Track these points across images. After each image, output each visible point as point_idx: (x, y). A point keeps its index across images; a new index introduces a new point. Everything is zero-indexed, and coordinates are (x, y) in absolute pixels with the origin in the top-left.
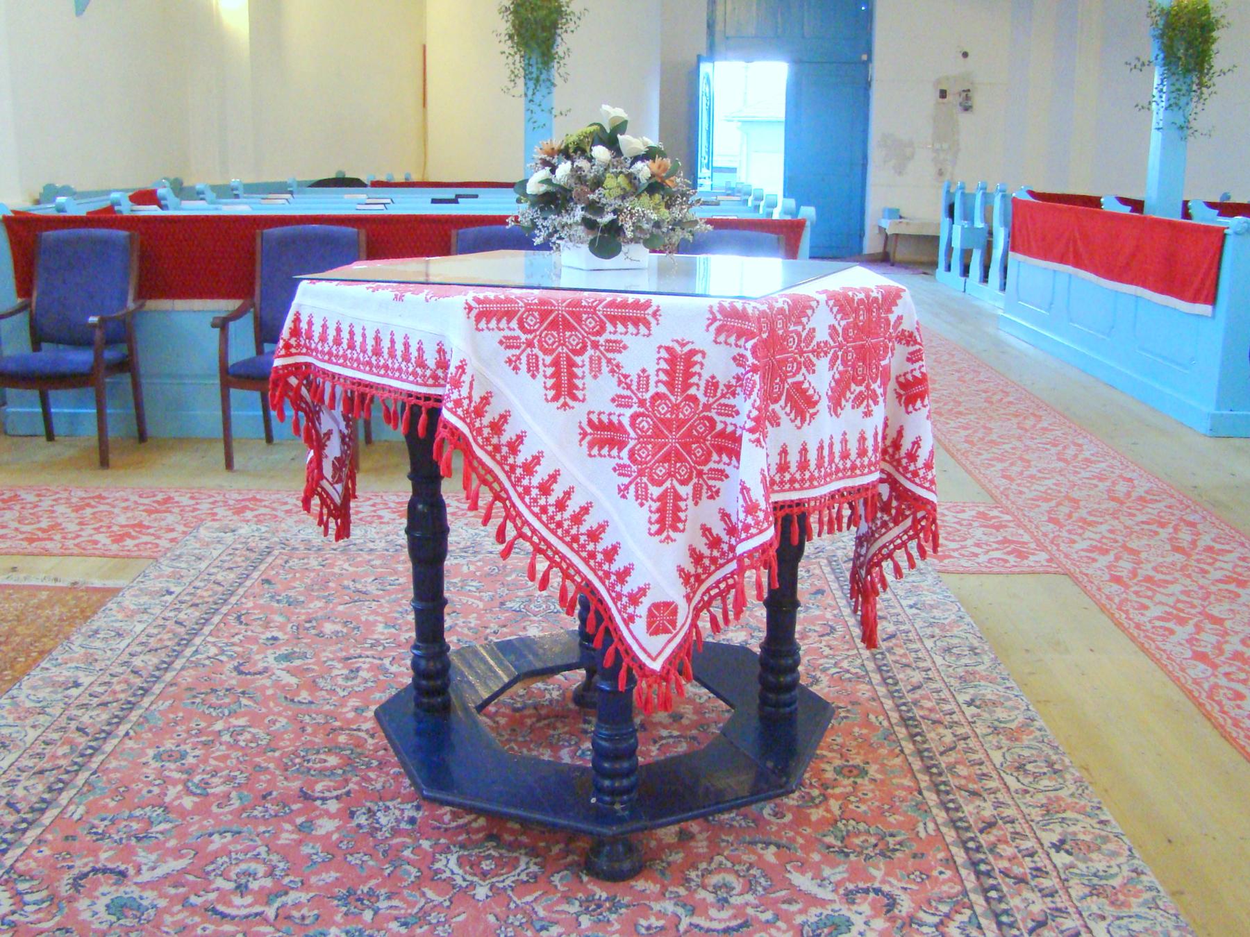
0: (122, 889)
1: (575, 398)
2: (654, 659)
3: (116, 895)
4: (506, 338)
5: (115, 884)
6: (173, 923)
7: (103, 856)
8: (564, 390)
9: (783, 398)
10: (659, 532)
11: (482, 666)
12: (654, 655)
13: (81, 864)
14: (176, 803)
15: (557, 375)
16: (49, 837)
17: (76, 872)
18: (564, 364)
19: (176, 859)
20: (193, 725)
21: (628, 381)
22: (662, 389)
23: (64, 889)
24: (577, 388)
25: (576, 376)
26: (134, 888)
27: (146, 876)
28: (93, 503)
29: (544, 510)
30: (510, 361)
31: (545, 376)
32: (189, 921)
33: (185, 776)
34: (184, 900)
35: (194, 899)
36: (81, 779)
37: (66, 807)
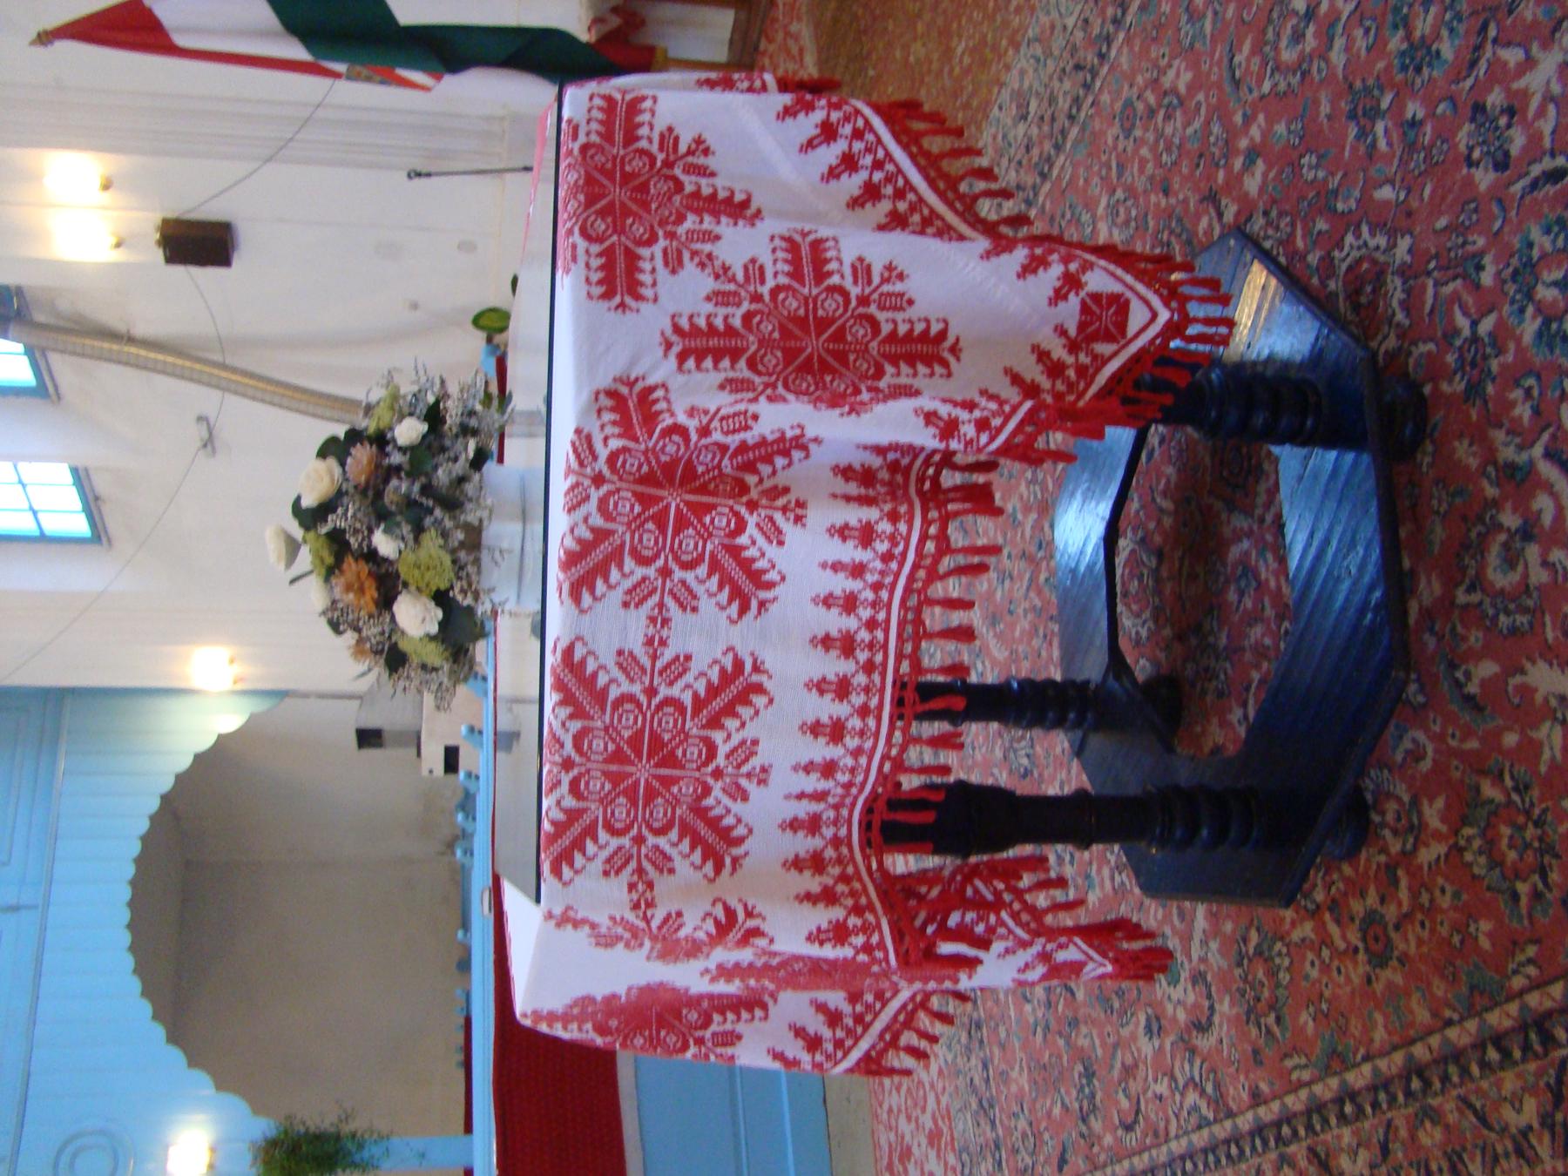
25: (709, 684)
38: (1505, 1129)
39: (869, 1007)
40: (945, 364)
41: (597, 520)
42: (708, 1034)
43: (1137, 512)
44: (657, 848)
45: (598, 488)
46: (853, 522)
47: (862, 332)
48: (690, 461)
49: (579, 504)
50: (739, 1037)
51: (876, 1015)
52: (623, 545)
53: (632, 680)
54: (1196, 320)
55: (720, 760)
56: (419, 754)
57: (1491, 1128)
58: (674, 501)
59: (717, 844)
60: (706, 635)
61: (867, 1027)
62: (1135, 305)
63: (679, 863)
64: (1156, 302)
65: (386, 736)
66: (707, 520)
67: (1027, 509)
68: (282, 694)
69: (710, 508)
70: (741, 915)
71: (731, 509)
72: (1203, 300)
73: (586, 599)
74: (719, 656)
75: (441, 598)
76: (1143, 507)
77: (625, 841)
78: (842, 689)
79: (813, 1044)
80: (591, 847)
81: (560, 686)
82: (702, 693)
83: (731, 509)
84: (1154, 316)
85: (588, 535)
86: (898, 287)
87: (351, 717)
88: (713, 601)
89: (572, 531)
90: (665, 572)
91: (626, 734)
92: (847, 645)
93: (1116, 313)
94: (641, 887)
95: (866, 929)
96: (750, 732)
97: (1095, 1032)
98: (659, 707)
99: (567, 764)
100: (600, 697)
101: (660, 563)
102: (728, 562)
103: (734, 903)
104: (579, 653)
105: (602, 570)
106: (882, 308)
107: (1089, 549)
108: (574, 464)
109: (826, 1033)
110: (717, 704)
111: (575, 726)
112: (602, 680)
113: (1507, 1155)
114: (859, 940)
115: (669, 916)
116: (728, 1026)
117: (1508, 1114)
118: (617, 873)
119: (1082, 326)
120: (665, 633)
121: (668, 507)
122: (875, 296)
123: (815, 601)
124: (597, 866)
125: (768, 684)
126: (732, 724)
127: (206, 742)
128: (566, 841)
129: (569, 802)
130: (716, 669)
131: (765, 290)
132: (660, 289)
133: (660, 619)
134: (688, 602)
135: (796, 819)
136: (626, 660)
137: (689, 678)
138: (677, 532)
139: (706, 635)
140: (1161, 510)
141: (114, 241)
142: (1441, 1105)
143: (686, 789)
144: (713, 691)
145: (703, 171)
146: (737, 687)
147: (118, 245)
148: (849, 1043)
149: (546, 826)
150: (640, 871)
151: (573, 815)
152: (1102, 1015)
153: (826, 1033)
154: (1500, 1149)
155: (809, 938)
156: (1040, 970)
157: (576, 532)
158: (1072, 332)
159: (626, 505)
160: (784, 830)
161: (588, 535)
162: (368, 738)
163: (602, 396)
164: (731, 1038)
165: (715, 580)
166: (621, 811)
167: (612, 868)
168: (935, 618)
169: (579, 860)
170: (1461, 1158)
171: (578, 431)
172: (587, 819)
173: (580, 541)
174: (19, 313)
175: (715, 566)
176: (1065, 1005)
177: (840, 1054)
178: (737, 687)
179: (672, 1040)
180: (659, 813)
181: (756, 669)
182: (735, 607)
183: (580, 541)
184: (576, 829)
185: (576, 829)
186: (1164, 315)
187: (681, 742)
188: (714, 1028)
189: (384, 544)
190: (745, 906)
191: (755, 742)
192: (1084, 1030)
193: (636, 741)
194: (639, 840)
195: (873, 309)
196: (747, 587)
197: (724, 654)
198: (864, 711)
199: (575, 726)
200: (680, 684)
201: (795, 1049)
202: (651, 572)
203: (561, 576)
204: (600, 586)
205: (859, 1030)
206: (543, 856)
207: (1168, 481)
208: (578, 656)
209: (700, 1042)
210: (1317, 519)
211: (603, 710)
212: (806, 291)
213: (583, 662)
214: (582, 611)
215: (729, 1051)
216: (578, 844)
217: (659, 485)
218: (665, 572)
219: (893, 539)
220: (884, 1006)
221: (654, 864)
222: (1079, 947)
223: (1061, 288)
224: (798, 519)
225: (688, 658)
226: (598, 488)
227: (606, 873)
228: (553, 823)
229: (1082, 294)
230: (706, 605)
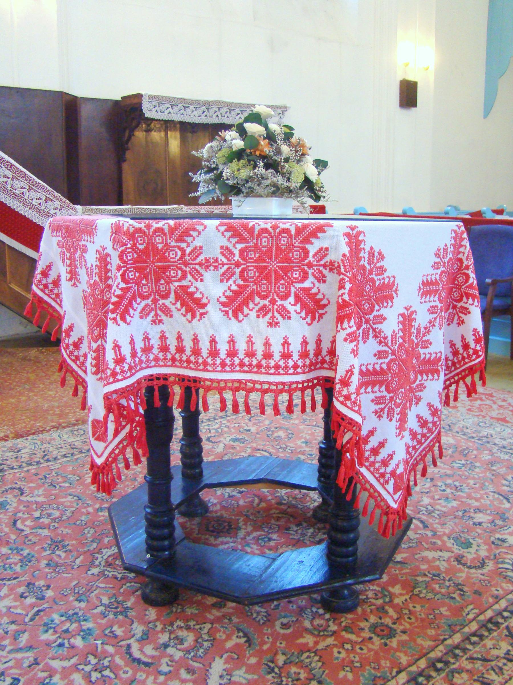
0: (461, 552)
2: (99, 457)
3: (465, 550)
4: (227, 248)
5: (464, 556)
6: (446, 529)
7: (463, 575)
8: (236, 304)
9: (256, 232)
12: (99, 454)
13: (477, 574)
14: (404, 592)
16: (491, 600)
17: (480, 571)
19: (426, 557)
20: (343, 655)
22: (240, 246)
23: (490, 566)
26: (454, 550)
27: (446, 555)
28: (484, 398)
29: (188, 361)
32: (439, 526)
33: (387, 607)
34: (435, 535)
35: (430, 534)
36: (457, 638)
37: (474, 619)
38: (498, 657)
40: (412, 313)
57: (493, 661)
60: (212, 287)
90: (238, 265)
113: (505, 664)
117: (495, 652)
125: (195, 321)
133: (207, 264)
134: (226, 276)
135: (198, 341)
139: (212, 287)
142: (460, 666)
145: (445, 250)
146: (193, 305)
154: (500, 664)
168: (241, 396)
170: (484, 678)
178: (193, 305)
181: (202, 314)
210: (277, 570)
228: (253, 227)
230: (225, 286)
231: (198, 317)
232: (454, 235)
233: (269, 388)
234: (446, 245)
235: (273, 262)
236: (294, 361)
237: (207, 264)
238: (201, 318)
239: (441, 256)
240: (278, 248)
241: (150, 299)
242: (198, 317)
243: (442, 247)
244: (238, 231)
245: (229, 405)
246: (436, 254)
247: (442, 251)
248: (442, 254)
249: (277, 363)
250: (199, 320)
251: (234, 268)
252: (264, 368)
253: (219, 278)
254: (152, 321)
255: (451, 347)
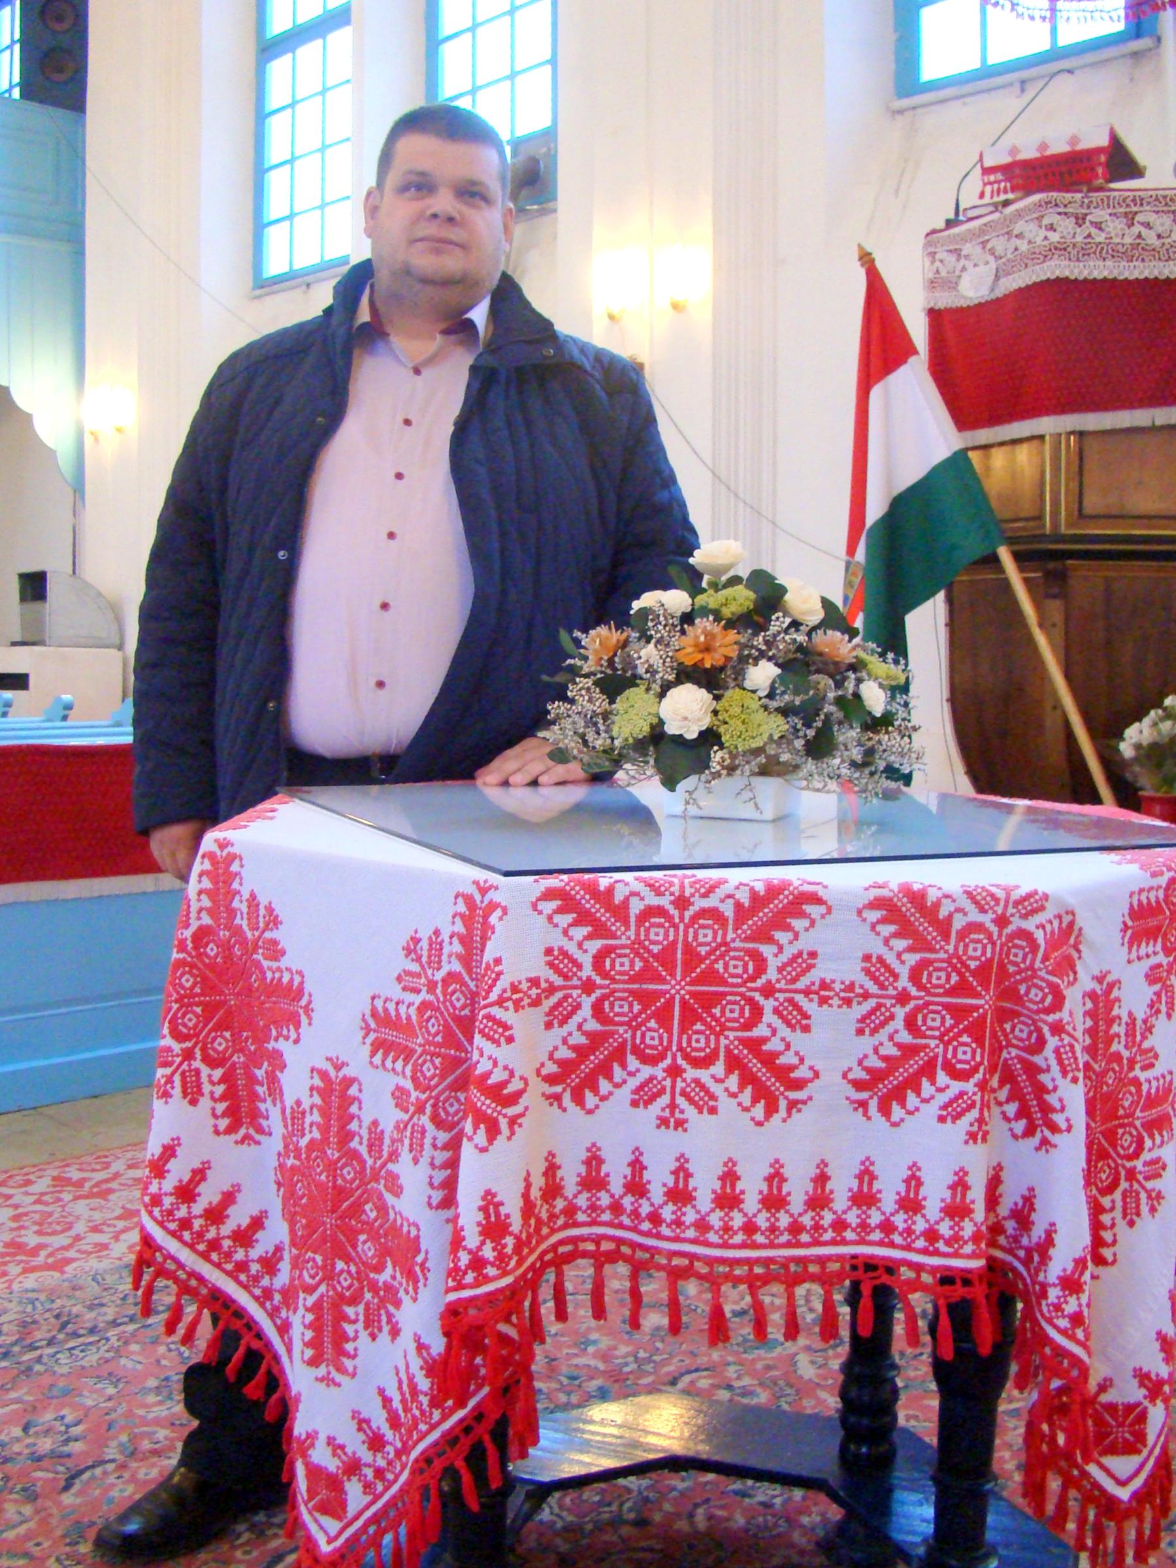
1: (799, 1084)
8: (772, 1082)
10: (858, 1085)
11: (513, 597)
15: (748, 1079)
18: (932, 933)
21: (858, 990)
24: (903, 1103)
25: (776, 1054)
30: (663, 1122)
31: (796, 936)
39: (228, 1255)
41: (958, 923)
42: (197, 1064)
43: (674, 1489)
44: (578, 1007)
45: (993, 921)
46: (970, 1195)
47: (1104, 1176)
48: (1018, 1014)
49: (976, 903)
50: (194, 1102)
51: (218, 1266)
52: (932, 950)
53: (780, 970)
54: (1120, 1530)
55: (691, 1073)
56: (14, 644)
58: (984, 1002)
59: (578, 1077)
60: (831, 1046)
61: (205, 1256)
62: (1134, 1460)
63: (558, 1033)
64: (1138, 1482)
65: (37, 605)
66: (965, 1038)
67: (605, 1357)
68: (79, 489)
69: (979, 1041)
70: (511, 1111)
71: (981, 1063)
72: (1140, 1533)
73: (874, 915)
74: (807, 1063)
75: (710, 737)
76: (682, 1494)
77: (587, 971)
78: (774, 1201)
79: (186, 1193)
80: (580, 932)
81: (774, 891)
82: (766, 1047)
83: (981, 1063)
84: (1122, 1483)
85: (943, 913)
86: (1144, 1209)
87: (55, 565)
88: (870, 1052)
89: (947, 896)
91: (720, 966)
92: (818, 1201)
93: (1126, 1440)
94: (534, 992)
95: (502, 1258)
96: (725, 1104)
97: (32, 1525)
98: (751, 1001)
99: (682, 902)
100: (763, 935)
101: (914, 992)
102: (913, 1065)
103: (524, 1101)
104: (813, 910)
105: (906, 930)
106: (1124, 1195)
107: (652, 1440)
108: (1016, 895)
109: (198, 1208)
110: (755, 1065)
111: (728, 910)
112: (782, 937)
114: (488, 1252)
115: (506, 1027)
116: (207, 1088)
118: (551, 965)
119: (1111, 1407)
120: (836, 1002)
121: (977, 995)
122: (1136, 1186)
123: (914, 1166)
124: (557, 940)
125: (776, 1118)
126: (733, 1082)
127: (22, 399)
128: (589, 904)
129: (636, 907)
130: (795, 1060)
131: (1137, 1072)
132: (1136, 963)
136: (805, 961)
137: (784, 1031)
138: (946, 1006)
139: (831, 1046)
140: (691, 1515)
141: (616, 313)
143: (653, 1037)
144: (769, 1060)
145: (436, 945)
147: (611, 317)
148: (187, 1236)
149: (604, 881)
150: (552, 989)
151: (620, 912)
152: (59, 1533)
153: (198, 1208)
155: (489, 1196)
156: (332, 1464)
157: (944, 901)
158: (1104, 1398)
159: (976, 954)
160: (589, 1150)
161: (943, 913)
162: (34, 586)
163: (1070, 917)
164: (192, 1094)
165: (894, 1052)
166: (622, 965)
167: (557, 959)
169: (565, 920)
171: (1046, 897)
172: (616, 927)
173: (937, 905)
174: (521, 210)
175: (908, 1051)
176: (46, 1481)
177: (173, 1226)
178: (772, 1084)
179: (191, 1021)
180: (621, 1007)
181: (793, 1105)
182: (862, 1075)
183: (937, 905)
184: (603, 915)
185: (603, 915)
186: (1124, 1494)
187: (710, 1027)
188: (205, 1071)
189: (762, 674)
190: (522, 1115)
191: (713, 1111)
192: (27, 1510)
193: (711, 976)
194: (588, 987)
195: (1124, 1185)
196: (885, 1087)
197: (811, 1068)
198: (750, 1228)
199: (728, 910)
200: (777, 1022)
201: (179, 1170)
202: (904, 982)
203: (894, 886)
204: (887, 929)
205: (201, 1247)
206: (565, 877)
207: (728, 1519)
208: (808, 908)
209: (188, 1055)
211: (747, 939)
212: (1138, 1114)
213: (802, 915)
214: (859, 912)
215: (177, 1091)
216: (584, 918)
217: (999, 983)
218: (903, 998)
219: (955, 1239)
220: (228, 1273)
221: (559, 1004)
222: (367, 1507)
223: (1150, 1379)
224: (972, 1136)
225: (806, 1029)
226: (993, 921)
227: (549, 951)
228: (610, 890)
229: (1146, 1403)
231: (783, 1112)
232: (462, 908)
233: (196, 1289)
234: (437, 933)
235: (678, 983)
236: (745, 1215)
237: (823, 992)
238: (789, 1114)
239: (424, 959)
240: (689, 950)
241: (973, 1081)
242: (783, 1112)
243: (425, 934)
244: (912, 924)
245: (776, 1319)
246: (408, 951)
247: (425, 944)
248: (425, 953)
249: (887, 1220)
250: (784, 1120)
251: (893, 1006)
252: (901, 1234)
253: (854, 1026)
254: (659, 1118)
255: (953, 1187)
